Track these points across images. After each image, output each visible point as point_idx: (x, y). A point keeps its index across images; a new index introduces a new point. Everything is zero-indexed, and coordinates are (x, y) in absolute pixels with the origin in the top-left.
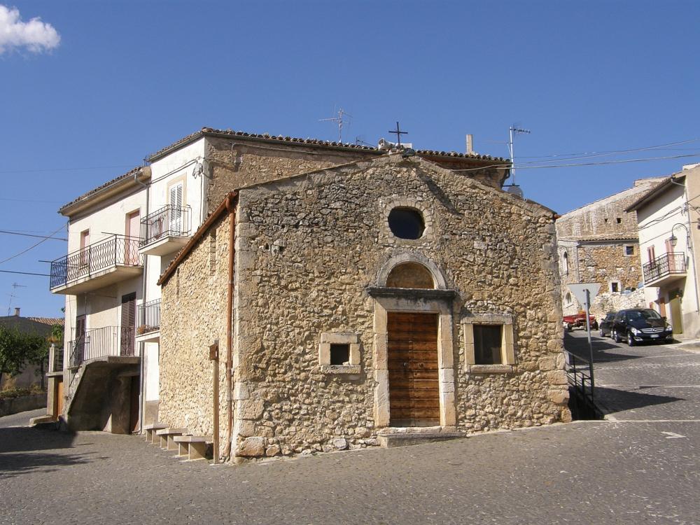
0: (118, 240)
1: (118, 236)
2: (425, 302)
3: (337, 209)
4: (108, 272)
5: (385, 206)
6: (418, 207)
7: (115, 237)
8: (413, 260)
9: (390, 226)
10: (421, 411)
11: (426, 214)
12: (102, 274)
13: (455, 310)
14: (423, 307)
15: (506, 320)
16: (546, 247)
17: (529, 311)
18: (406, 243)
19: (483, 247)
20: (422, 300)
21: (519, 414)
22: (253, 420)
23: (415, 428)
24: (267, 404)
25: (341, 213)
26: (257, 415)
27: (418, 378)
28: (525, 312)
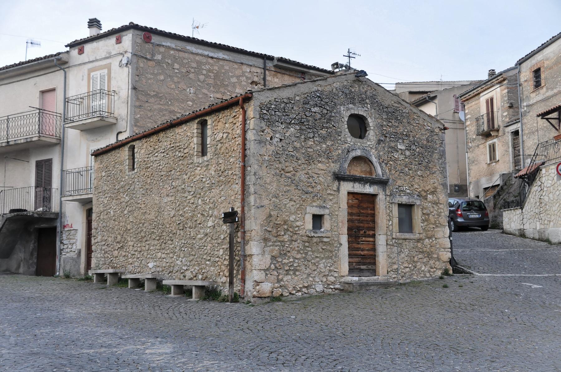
0: (41, 114)
1: (41, 111)
2: (370, 186)
3: (315, 113)
4: (29, 140)
5: (345, 112)
6: (365, 115)
7: (38, 111)
8: (365, 155)
9: (348, 128)
10: (365, 265)
11: (371, 121)
12: (22, 141)
13: (387, 193)
14: (369, 189)
15: (416, 201)
16: (439, 150)
17: (429, 196)
18: (359, 142)
19: (403, 148)
20: (368, 184)
21: (423, 269)
22: (264, 270)
23: (363, 278)
24: (273, 258)
25: (319, 116)
26: (267, 267)
27: (363, 241)
28: (426, 196)
